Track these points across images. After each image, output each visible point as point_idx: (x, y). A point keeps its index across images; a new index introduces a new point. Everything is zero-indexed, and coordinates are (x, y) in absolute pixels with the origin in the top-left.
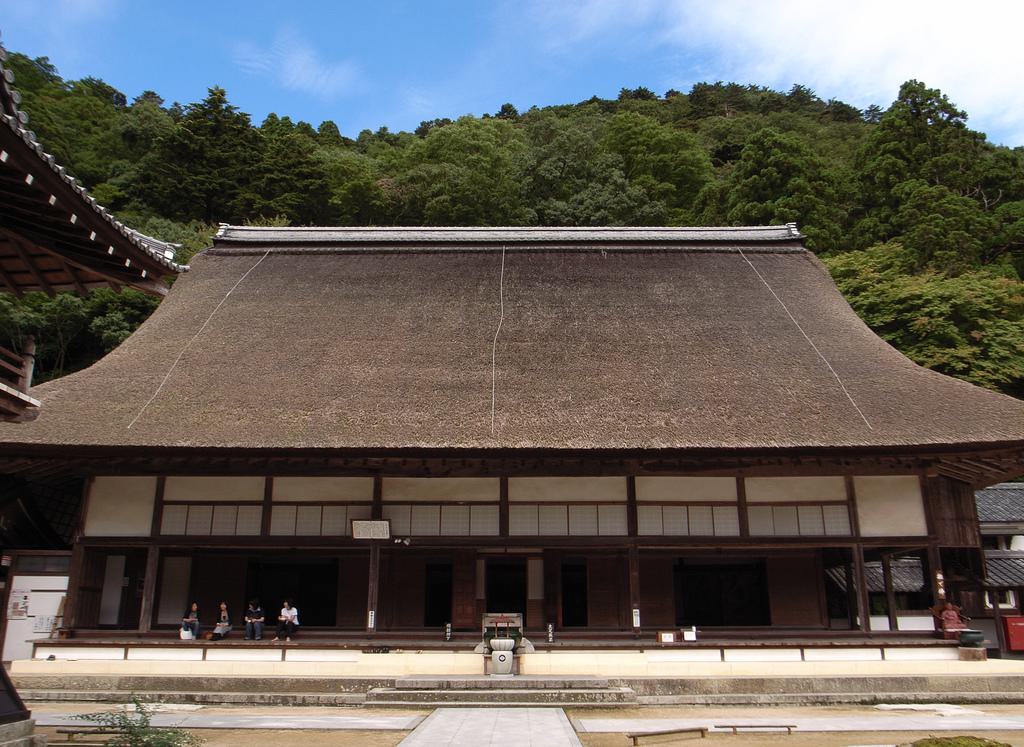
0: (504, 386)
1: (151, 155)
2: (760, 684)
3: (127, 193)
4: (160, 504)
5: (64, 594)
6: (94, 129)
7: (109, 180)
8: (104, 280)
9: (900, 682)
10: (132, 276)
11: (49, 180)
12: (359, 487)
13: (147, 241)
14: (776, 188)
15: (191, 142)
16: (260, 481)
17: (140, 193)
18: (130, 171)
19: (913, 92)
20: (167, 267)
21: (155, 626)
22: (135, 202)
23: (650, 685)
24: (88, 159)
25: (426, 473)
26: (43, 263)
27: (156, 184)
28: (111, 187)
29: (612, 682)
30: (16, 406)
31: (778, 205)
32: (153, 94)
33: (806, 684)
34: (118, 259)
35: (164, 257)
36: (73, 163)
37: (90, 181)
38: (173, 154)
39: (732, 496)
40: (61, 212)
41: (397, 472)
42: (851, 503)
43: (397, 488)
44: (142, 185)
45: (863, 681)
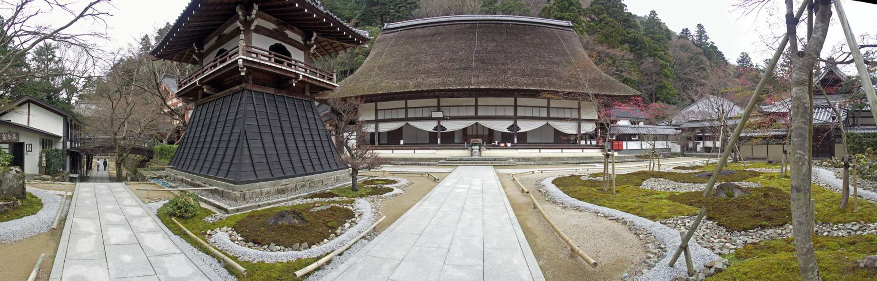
0: (476, 68)
2: (550, 159)
4: (377, 110)
9: (586, 158)
10: (357, 43)
11: (338, 24)
12: (433, 102)
14: (567, 9)
16: (403, 102)
17: (362, 20)
18: (358, 13)
21: (379, 144)
23: (519, 159)
24: (347, 13)
25: (453, 97)
26: (334, 45)
28: (354, 21)
29: (508, 158)
31: (567, 15)
33: (562, 159)
37: (349, 20)
39: (546, 105)
41: (444, 97)
42: (579, 109)
43: (444, 102)
45: (577, 158)
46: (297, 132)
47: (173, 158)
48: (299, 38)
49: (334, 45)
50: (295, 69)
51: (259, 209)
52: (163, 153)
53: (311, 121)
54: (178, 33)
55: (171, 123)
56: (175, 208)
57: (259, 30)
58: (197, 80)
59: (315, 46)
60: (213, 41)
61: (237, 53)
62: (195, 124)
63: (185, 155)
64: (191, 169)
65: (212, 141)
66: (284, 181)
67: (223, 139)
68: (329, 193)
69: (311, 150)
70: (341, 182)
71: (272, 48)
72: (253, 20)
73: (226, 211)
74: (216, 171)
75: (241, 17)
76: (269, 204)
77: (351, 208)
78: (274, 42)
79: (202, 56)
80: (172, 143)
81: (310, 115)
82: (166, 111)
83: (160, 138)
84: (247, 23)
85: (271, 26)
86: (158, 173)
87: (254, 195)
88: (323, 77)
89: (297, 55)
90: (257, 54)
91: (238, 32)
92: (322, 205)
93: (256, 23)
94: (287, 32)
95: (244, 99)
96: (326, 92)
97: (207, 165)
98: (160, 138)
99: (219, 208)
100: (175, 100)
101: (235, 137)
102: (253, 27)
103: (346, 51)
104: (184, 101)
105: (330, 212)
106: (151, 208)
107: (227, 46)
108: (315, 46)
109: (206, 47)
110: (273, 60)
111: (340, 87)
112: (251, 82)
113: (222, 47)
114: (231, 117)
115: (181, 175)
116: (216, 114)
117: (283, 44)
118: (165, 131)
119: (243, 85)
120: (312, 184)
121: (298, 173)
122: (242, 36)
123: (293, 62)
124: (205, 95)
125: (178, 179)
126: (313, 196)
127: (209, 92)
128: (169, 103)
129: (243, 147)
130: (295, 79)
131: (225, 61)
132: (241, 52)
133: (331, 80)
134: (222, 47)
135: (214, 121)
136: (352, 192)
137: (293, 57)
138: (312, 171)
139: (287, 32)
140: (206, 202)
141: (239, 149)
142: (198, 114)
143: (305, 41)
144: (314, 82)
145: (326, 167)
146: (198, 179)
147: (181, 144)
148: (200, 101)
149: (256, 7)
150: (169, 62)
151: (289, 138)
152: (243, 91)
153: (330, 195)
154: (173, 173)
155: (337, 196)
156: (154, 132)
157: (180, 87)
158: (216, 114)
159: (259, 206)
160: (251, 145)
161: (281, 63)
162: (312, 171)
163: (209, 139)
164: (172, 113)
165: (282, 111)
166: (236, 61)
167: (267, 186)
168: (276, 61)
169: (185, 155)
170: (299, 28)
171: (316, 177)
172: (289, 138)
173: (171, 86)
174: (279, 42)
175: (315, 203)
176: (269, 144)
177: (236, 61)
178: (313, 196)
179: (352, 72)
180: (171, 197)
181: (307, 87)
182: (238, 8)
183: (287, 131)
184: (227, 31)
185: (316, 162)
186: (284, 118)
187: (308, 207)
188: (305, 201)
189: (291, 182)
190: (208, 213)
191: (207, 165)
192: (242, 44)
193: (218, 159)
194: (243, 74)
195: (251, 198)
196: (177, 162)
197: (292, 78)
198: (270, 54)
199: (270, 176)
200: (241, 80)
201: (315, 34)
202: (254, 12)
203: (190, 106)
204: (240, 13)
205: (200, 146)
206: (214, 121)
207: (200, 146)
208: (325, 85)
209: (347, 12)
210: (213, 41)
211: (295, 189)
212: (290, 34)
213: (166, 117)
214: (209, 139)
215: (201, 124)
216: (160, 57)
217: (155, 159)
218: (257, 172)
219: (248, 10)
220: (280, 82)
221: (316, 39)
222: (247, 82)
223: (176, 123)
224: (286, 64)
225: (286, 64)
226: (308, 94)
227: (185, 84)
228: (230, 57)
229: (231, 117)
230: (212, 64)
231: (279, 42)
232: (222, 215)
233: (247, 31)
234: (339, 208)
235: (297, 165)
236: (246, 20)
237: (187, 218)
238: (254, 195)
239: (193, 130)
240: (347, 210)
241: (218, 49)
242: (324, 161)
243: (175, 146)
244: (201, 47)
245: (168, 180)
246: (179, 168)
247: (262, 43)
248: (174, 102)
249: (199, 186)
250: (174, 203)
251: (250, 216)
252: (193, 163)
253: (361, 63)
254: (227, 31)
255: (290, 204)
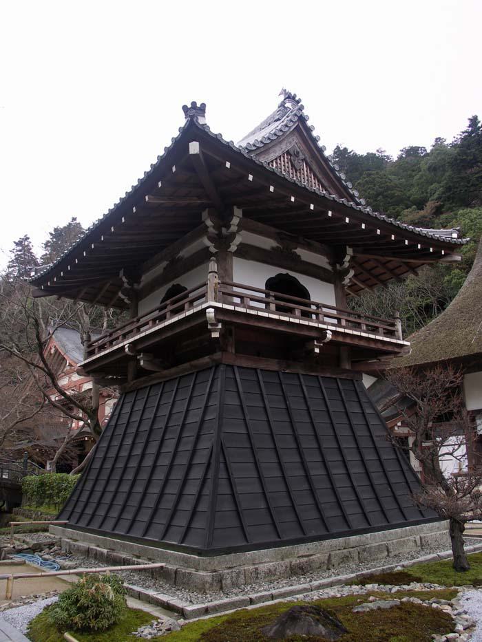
1: (447, 174)
3: (442, 202)
5: (190, 478)
6: (414, 173)
7: (430, 199)
8: (423, 264)
10: (437, 255)
13: (431, 232)
15: (467, 156)
17: (449, 198)
19: (115, 204)
20: (455, 244)
22: (447, 205)
26: (390, 266)
27: (455, 190)
30: (397, 348)
32: (440, 138)
34: (425, 249)
35: (452, 238)
36: (409, 197)
38: (459, 168)
40: (385, 236)
44: (448, 194)
46: (328, 444)
47: (66, 502)
48: (321, 261)
49: (390, 266)
50: (318, 320)
51: (250, 607)
52: (44, 493)
53: (357, 421)
54: (90, 252)
55: (65, 424)
56: (73, 609)
57: (246, 252)
58: (126, 342)
59: (352, 273)
60: (159, 269)
61: (203, 296)
62: (120, 431)
63: (97, 496)
64: (108, 527)
65: (154, 467)
66: (303, 549)
67: (177, 462)
68: (400, 574)
69: (360, 482)
70: (432, 550)
71: (272, 284)
72: (233, 236)
73: (182, 613)
74: (162, 528)
75: (211, 230)
76: (273, 597)
77: (447, 609)
78: (273, 272)
79: (137, 296)
80: (67, 469)
81: (354, 409)
82: (54, 398)
83: (39, 457)
84: (222, 241)
85: (268, 243)
86: (32, 540)
87: (242, 579)
88: (375, 330)
89: (322, 294)
90: (242, 297)
91: (204, 256)
92: (380, 598)
93: (238, 240)
94: (299, 251)
95: (218, 386)
96: (383, 359)
97: (144, 517)
98: (39, 457)
99: (168, 607)
100: (76, 378)
101: (201, 458)
102: (233, 248)
103: (416, 274)
104: (96, 382)
105: (397, 614)
106: (13, 621)
107: (188, 281)
108: (352, 273)
109: (146, 278)
110: (273, 307)
111: (409, 345)
112: (232, 350)
113: (175, 282)
114: (194, 418)
115: (87, 541)
116: (165, 411)
117: (292, 274)
118: (51, 443)
119: (217, 355)
120: (365, 554)
121: (334, 531)
122: (213, 266)
123: (314, 307)
124: (141, 372)
125: (78, 550)
126: (363, 580)
127: (149, 368)
128: (63, 382)
129: (216, 477)
130: (319, 340)
131: (181, 309)
132: (211, 294)
133: (391, 333)
134: (175, 282)
135: (161, 425)
136: (452, 572)
137: (312, 299)
138: (364, 526)
139: (299, 251)
140: (139, 596)
141: (209, 484)
142: (127, 409)
143: (333, 264)
144: (356, 342)
145: (376, 519)
146: (124, 547)
147: (86, 471)
148: (131, 383)
149: (238, 212)
150: (68, 301)
151: (312, 459)
152: (217, 366)
153: (402, 578)
154: (57, 533)
155: (419, 580)
156: (25, 445)
157: (91, 353)
158: (165, 411)
159: (251, 601)
160: (235, 475)
161: (289, 311)
162: (364, 526)
163: (148, 462)
164: (69, 404)
165: (296, 405)
166: (203, 311)
167: (267, 559)
168: (280, 309)
169: (97, 496)
170: (322, 242)
171: (373, 539)
172: (312, 459)
173: (70, 347)
174: (284, 271)
175: (369, 594)
176: (271, 472)
177: (203, 311)
178: (363, 580)
179: (442, 305)
180: (63, 588)
181: (344, 354)
182: (205, 214)
183: (308, 444)
184: (186, 252)
185: (370, 507)
186: (301, 418)
187: (348, 604)
188: (346, 591)
189: (316, 551)
190: (144, 618)
191: (144, 517)
192: (213, 280)
193: (168, 503)
194: (215, 335)
195: (235, 585)
196: (76, 511)
197: (313, 339)
198: (268, 296)
199: (274, 538)
200: (214, 345)
201: (350, 251)
202: (235, 221)
203: (109, 390)
204: (209, 223)
205: (130, 476)
206: (161, 425)
207: (130, 476)
208: (379, 346)
209: (414, 190)
210: (159, 269)
211: (328, 564)
212: (305, 255)
213: (57, 412)
214: (148, 462)
215: (133, 430)
216: (49, 291)
217: (25, 507)
218: (248, 530)
219: (223, 219)
220: (290, 347)
221: (352, 258)
222: (224, 350)
223: (77, 425)
224: (298, 313)
225: (298, 313)
226: (347, 366)
227: (102, 347)
228: (191, 302)
229: (194, 418)
230: (156, 314)
231: (284, 271)
232: (171, 621)
233: (223, 256)
234: (419, 607)
235: (331, 513)
236: (220, 234)
237: (100, 631)
238: (242, 579)
239: (116, 443)
240: (438, 613)
241: (169, 285)
242: (389, 505)
243: (73, 477)
244: (134, 278)
245: (56, 554)
246: (82, 524)
247: (251, 277)
248: (73, 382)
249: (125, 562)
250: (73, 601)
251: (231, 621)
252: (114, 513)
253: (459, 285)
254: (186, 252)
255: (315, 596)
